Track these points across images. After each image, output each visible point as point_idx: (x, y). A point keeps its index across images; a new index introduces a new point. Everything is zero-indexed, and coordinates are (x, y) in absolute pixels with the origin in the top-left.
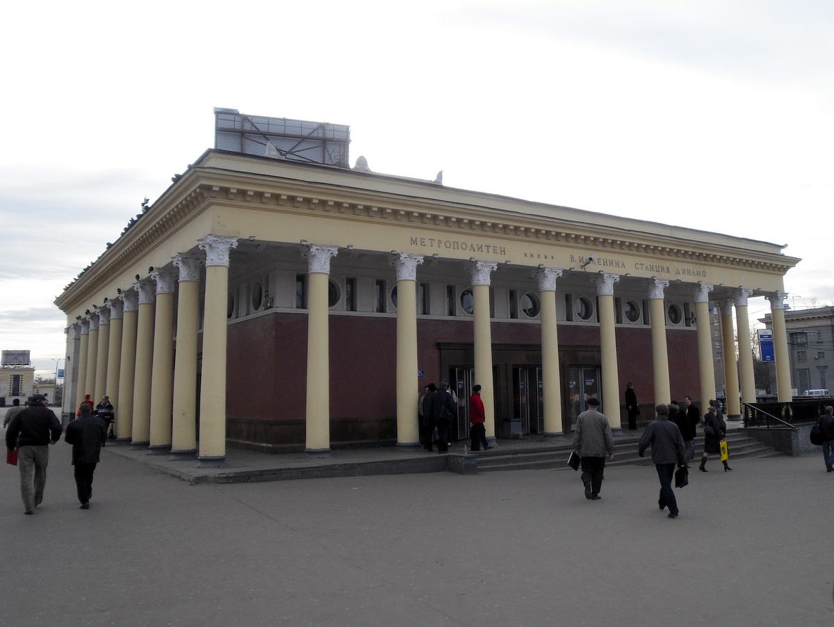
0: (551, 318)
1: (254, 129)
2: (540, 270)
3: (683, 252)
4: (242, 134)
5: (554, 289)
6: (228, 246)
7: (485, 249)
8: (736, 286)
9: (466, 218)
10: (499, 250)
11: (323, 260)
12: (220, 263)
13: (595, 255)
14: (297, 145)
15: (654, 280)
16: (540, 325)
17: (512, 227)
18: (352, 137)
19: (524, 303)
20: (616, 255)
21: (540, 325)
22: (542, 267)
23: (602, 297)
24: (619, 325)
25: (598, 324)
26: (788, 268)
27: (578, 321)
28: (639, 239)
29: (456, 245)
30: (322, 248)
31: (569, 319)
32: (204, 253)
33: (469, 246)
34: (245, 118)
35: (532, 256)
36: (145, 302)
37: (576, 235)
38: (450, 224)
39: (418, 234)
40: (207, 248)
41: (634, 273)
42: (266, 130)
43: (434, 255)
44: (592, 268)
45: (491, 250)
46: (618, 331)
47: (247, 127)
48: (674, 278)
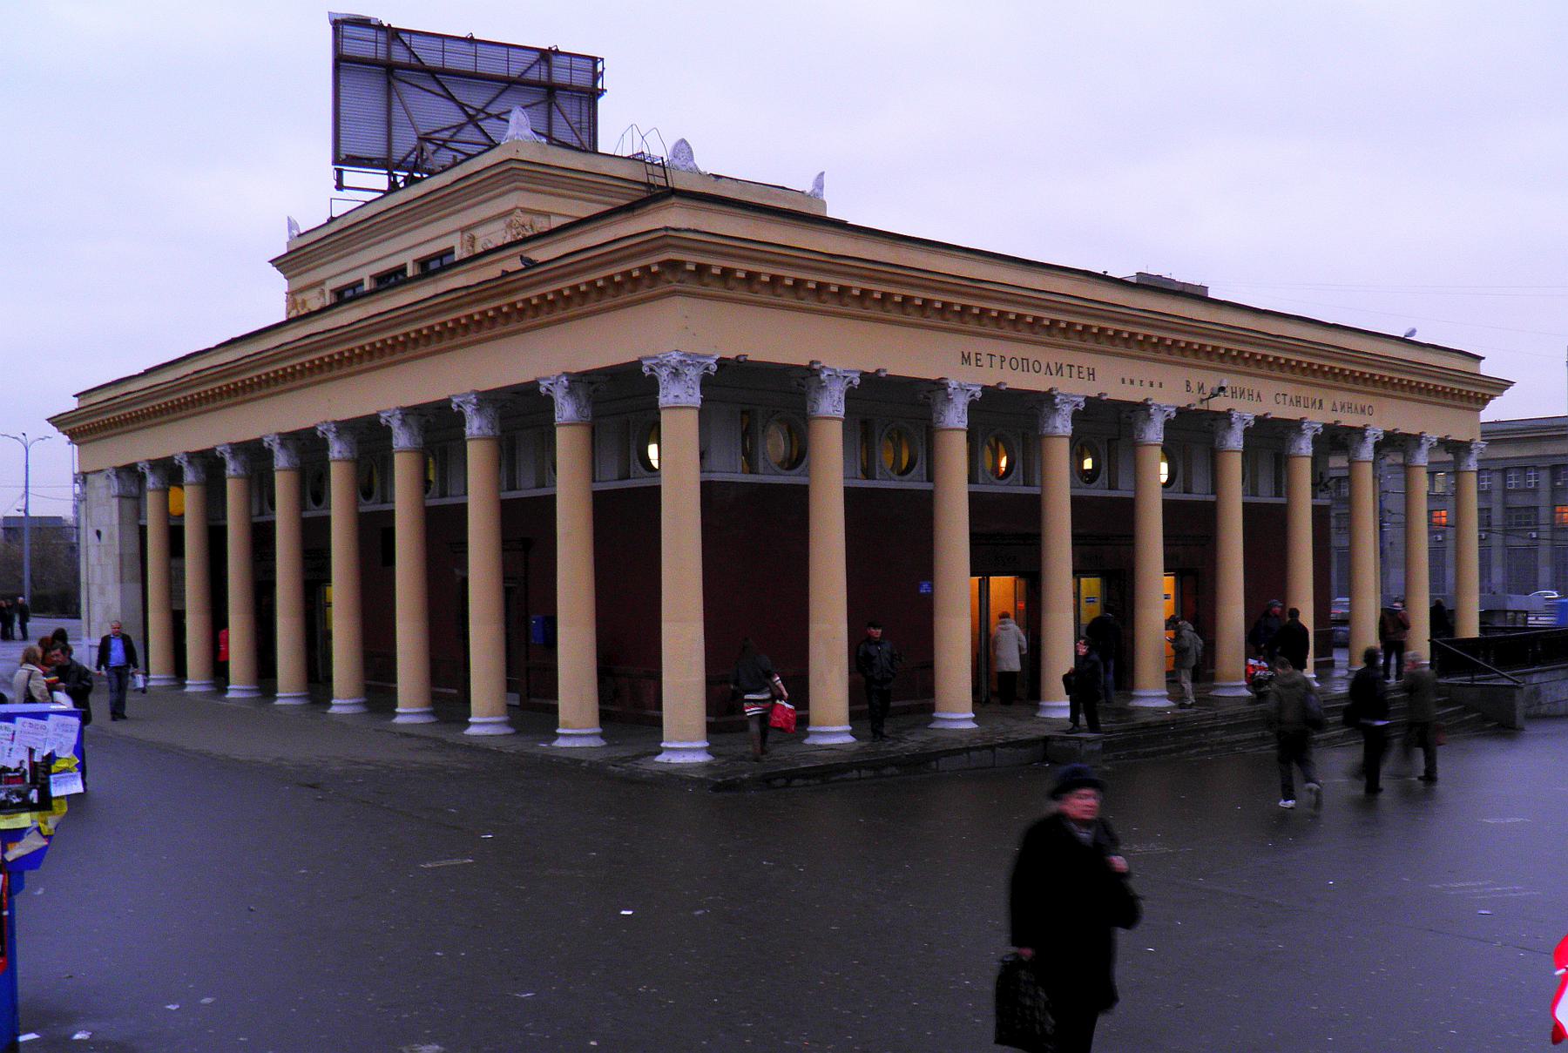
0: (676, 460)
1: (413, 61)
2: (938, 386)
3: (1012, 317)
4: (389, 71)
5: (964, 425)
6: (701, 371)
7: (1066, 370)
8: (1415, 432)
9: (766, 271)
10: (1085, 374)
11: (837, 395)
12: (683, 401)
13: (1227, 381)
14: (494, 99)
15: (1150, 406)
16: (931, 492)
17: (789, 282)
18: (609, 81)
19: (775, 445)
20: (1242, 378)
21: (931, 492)
22: (816, 366)
23: (817, 422)
24: (976, 488)
25: (928, 486)
26: (1492, 397)
27: (886, 482)
28: (774, 263)
29: (1025, 364)
30: (835, 376)
31: (868, 473)
32: (652, 385)
33: (1044, 367)
34: (394, 34)
35: (1132, 382)
36: (347, 454)
37: (818, 284)
38: (757, 287)
39: (973, 345)
40: (663, 374)
41: (1117, 391)
42: (567, 81)
43: (812, 362)
44: (1219, 404)
45: (997, 360)
46: (973, 497)
47: (400, 55)
48: (1330, 418)
